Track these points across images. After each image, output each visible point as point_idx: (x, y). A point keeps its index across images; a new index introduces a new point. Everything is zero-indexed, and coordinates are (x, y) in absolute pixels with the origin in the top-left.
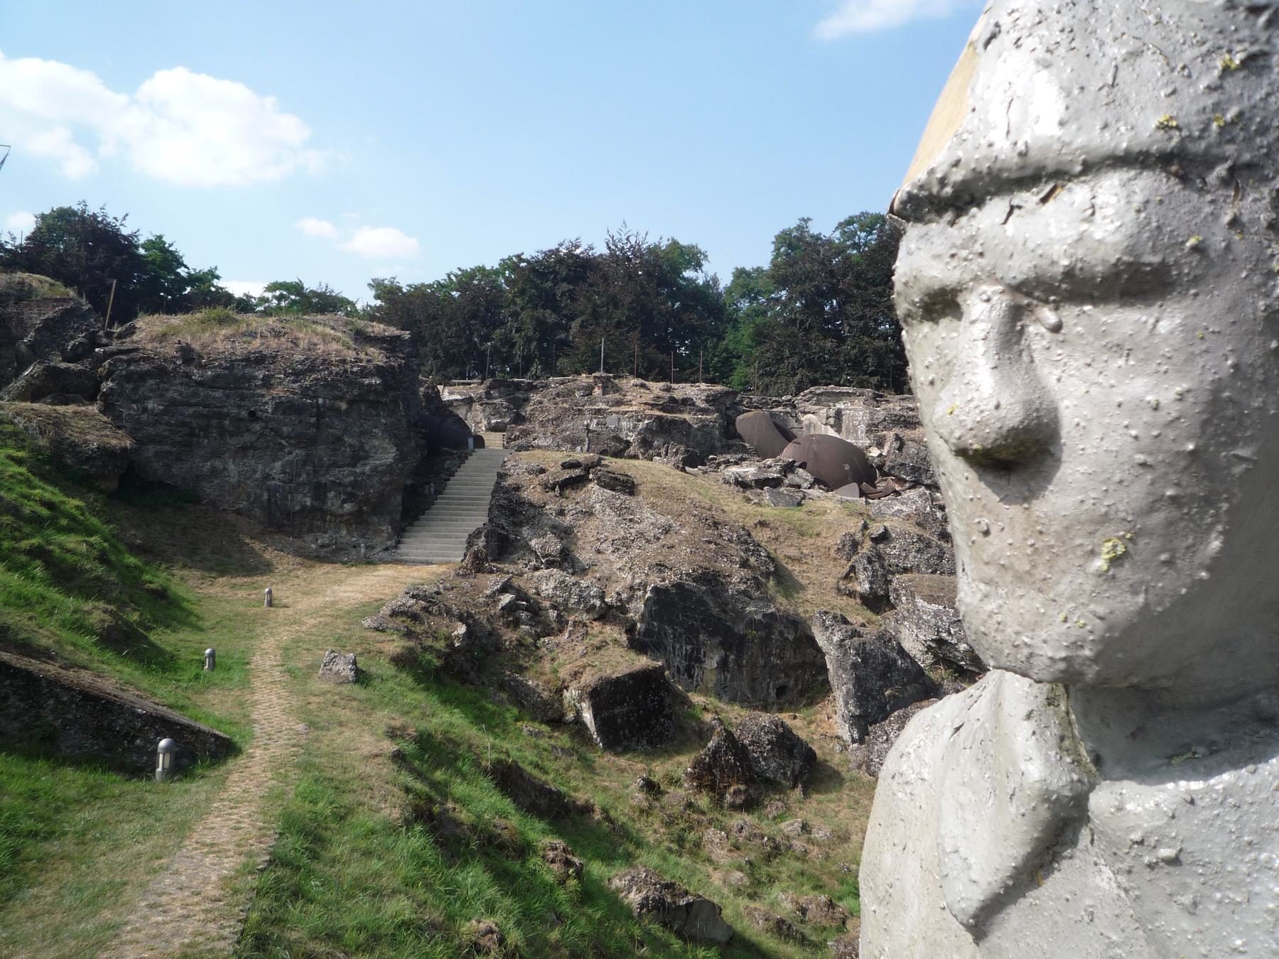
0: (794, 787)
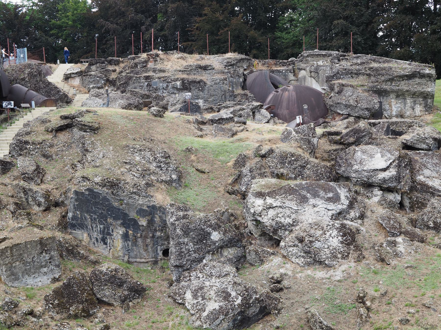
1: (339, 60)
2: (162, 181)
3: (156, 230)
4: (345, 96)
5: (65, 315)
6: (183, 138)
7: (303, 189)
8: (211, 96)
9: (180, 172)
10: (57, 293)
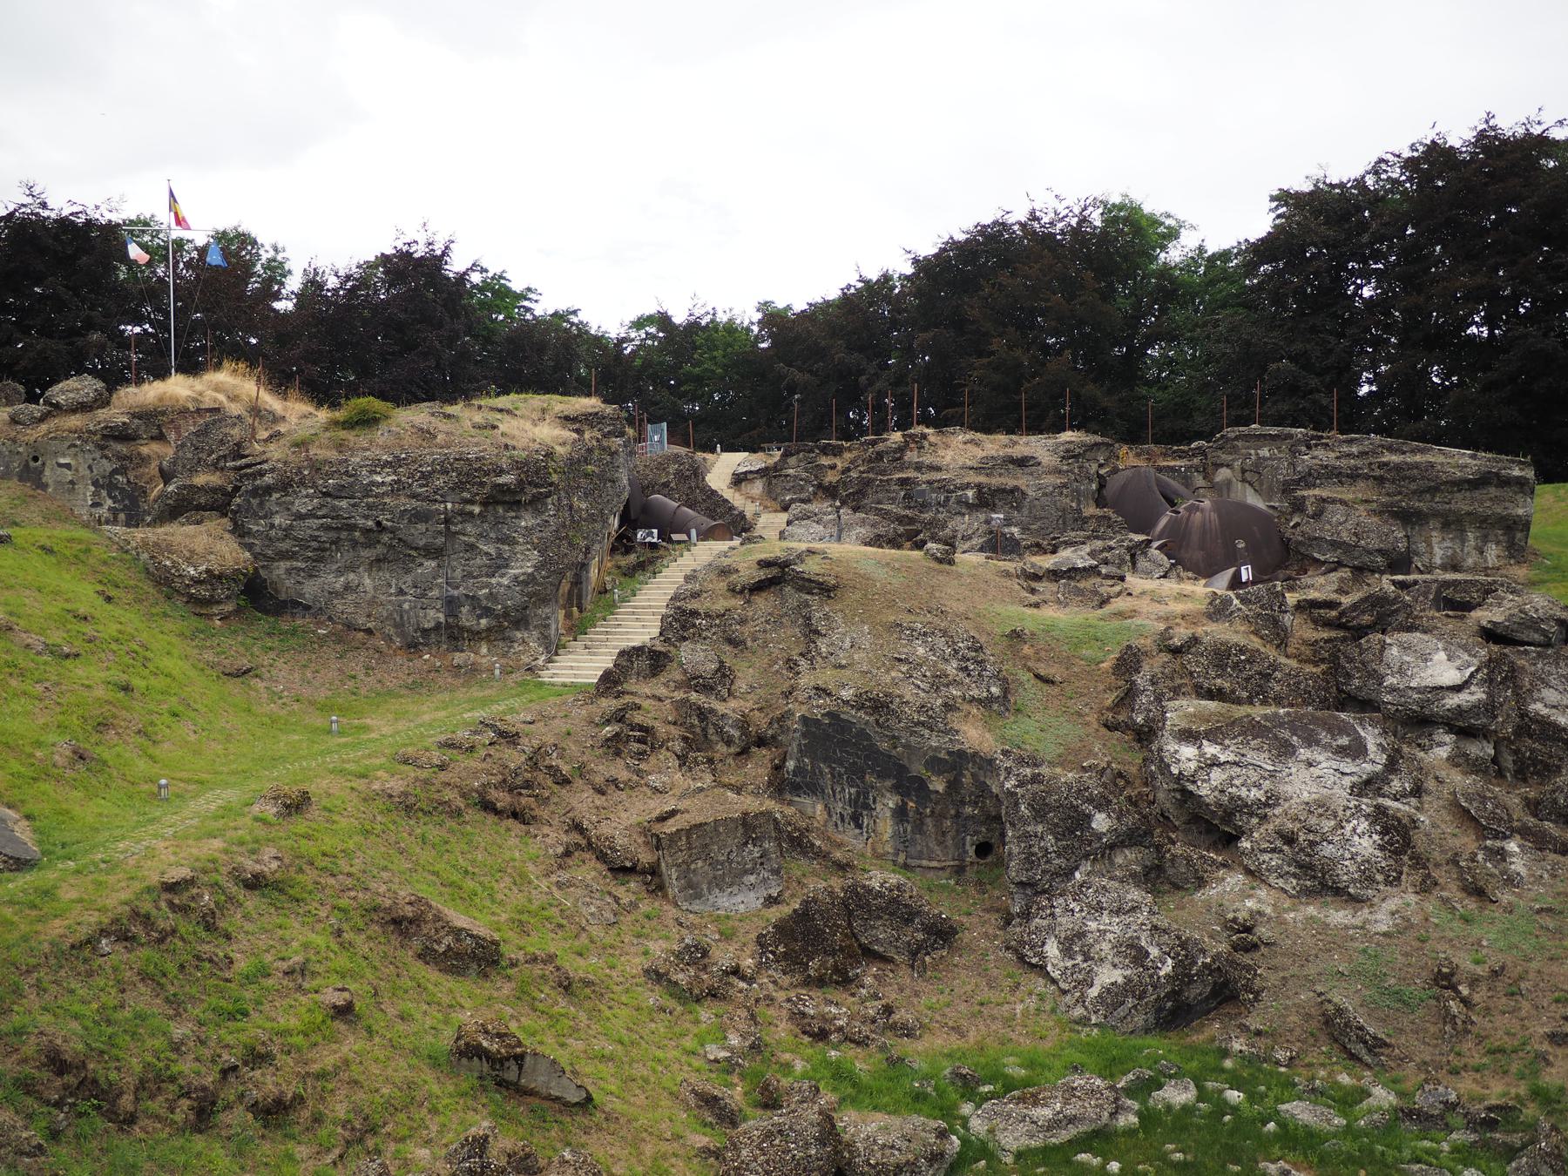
0: (111, 866)
1: (1309, 447)
2: (973, 699)
3: (963, 803)
4: (1329, 522)
5: (798, 978)
6: (999, 608)
7: (1281, 725)
8: (1036, 519)
9: (1005, 680)
10: (783, 930)
